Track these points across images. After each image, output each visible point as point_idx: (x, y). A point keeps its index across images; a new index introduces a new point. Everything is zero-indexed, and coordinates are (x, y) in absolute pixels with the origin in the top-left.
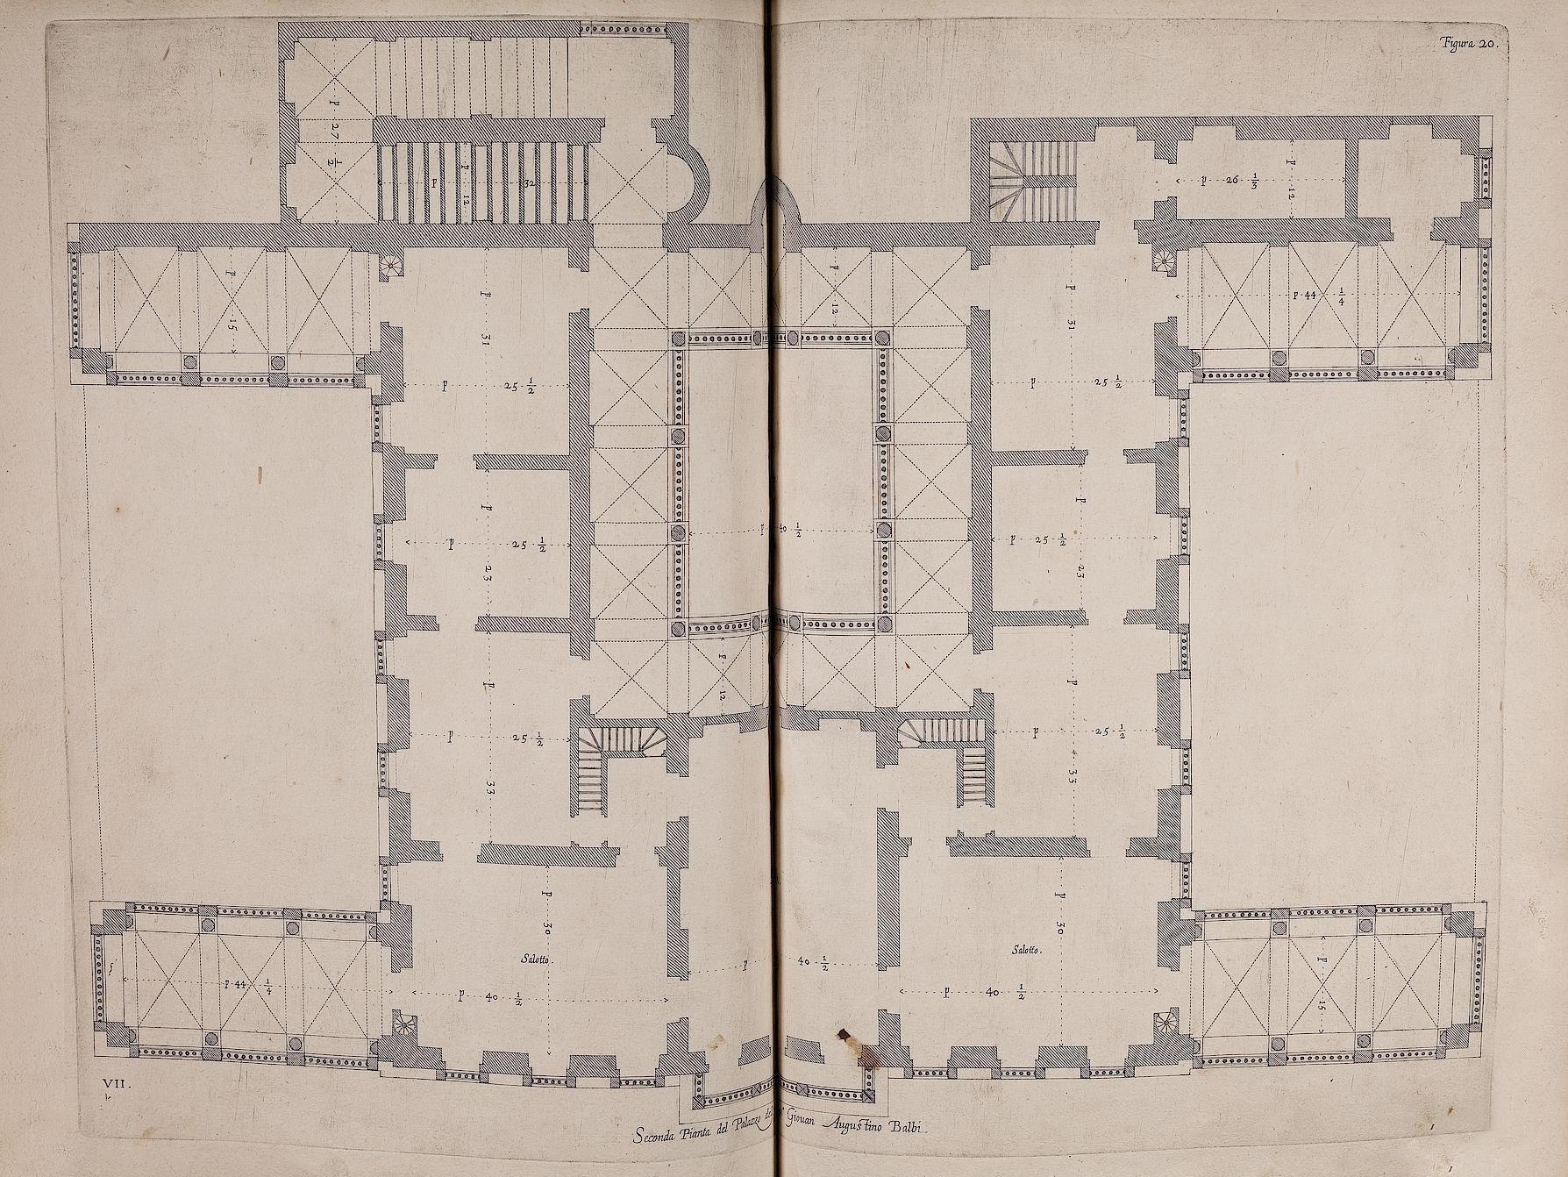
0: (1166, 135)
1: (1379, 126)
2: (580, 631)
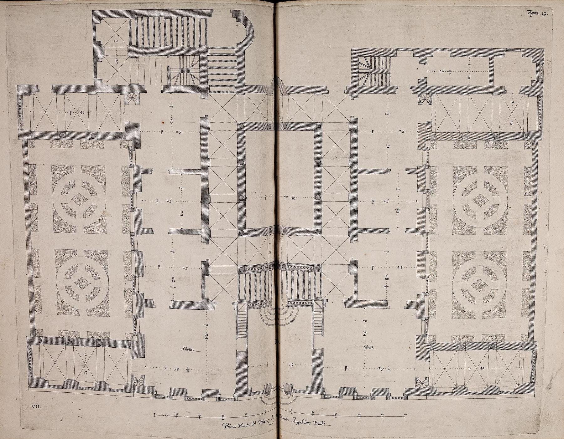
0: (423, 55)
1: (502, 52)
2: (205, 234)
